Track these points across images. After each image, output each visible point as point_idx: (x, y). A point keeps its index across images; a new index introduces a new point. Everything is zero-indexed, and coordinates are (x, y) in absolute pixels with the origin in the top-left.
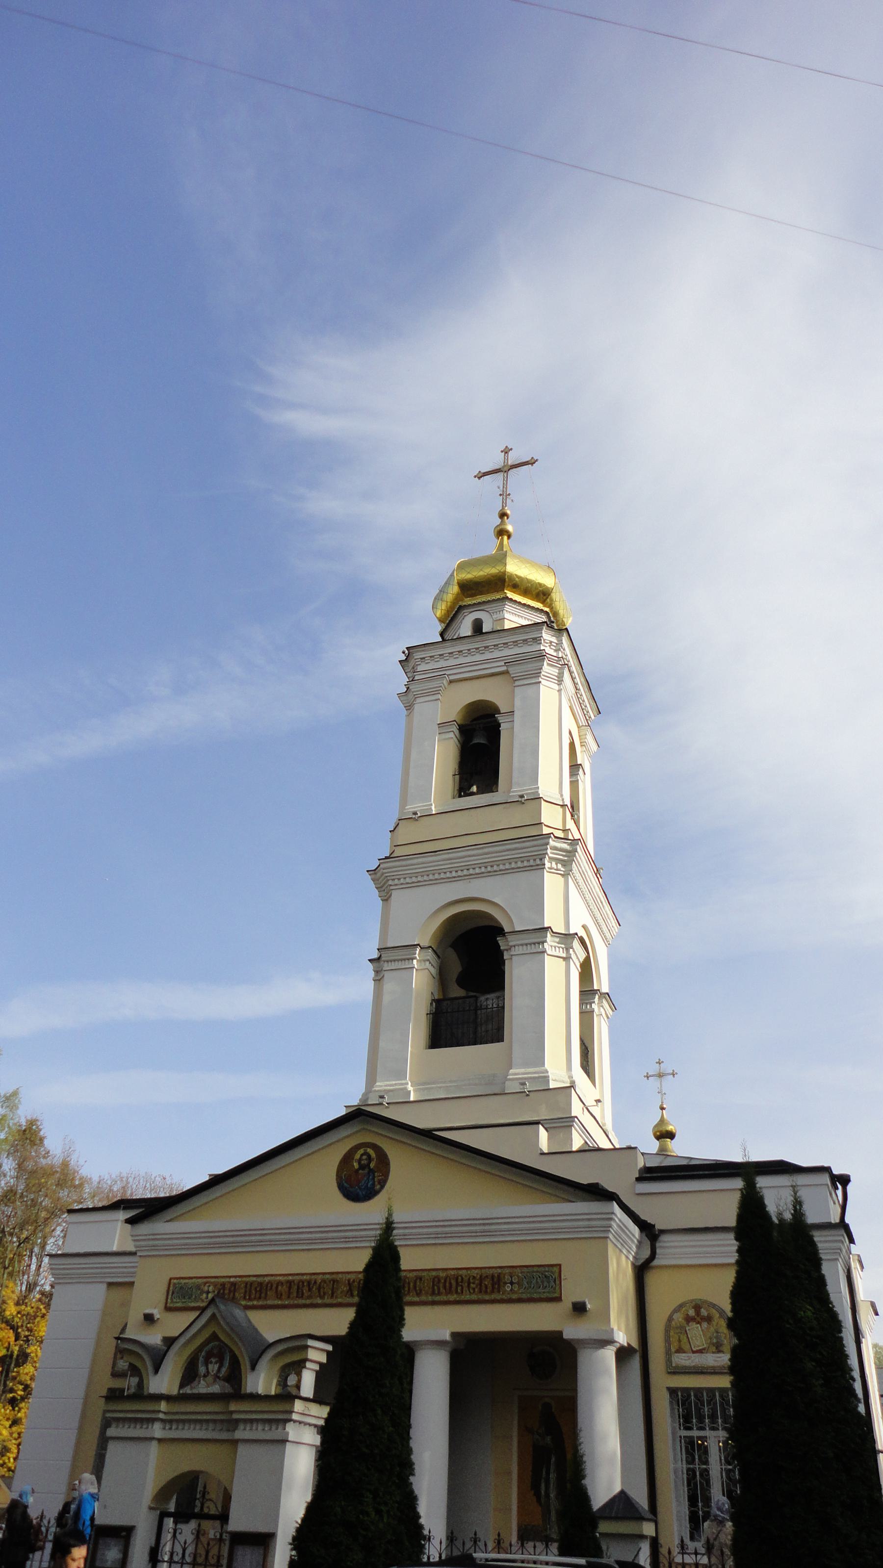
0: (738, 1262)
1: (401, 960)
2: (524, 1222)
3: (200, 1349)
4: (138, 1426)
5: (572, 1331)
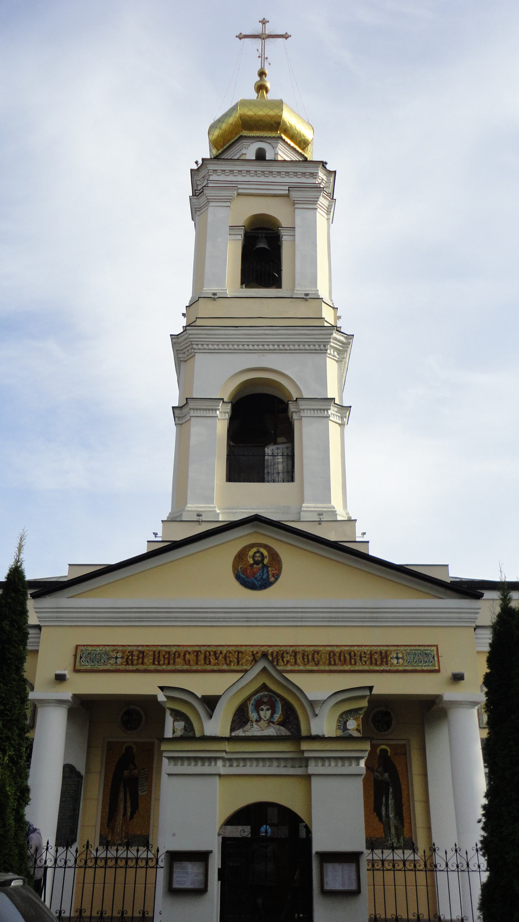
0: (490, 653)
1: (206, 410)
2: (407, 612)
3: (249, 699)
4: (207, 764)
5: (450, 694)
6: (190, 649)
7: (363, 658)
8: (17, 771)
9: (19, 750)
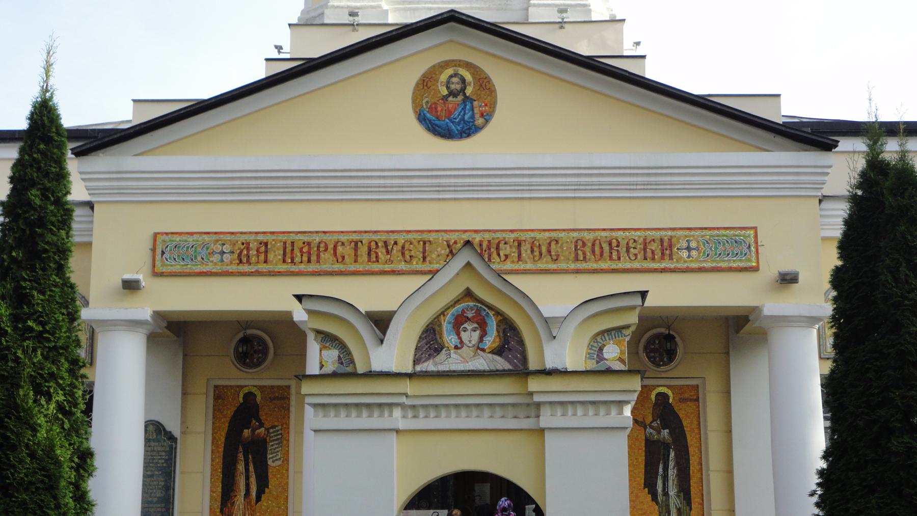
3: (443, 313)
5: (774, 305)
6: (343, 238)
7: (632, 250)
8: (71, 426)
9: (72, 395)
